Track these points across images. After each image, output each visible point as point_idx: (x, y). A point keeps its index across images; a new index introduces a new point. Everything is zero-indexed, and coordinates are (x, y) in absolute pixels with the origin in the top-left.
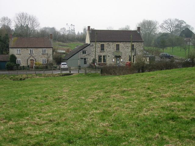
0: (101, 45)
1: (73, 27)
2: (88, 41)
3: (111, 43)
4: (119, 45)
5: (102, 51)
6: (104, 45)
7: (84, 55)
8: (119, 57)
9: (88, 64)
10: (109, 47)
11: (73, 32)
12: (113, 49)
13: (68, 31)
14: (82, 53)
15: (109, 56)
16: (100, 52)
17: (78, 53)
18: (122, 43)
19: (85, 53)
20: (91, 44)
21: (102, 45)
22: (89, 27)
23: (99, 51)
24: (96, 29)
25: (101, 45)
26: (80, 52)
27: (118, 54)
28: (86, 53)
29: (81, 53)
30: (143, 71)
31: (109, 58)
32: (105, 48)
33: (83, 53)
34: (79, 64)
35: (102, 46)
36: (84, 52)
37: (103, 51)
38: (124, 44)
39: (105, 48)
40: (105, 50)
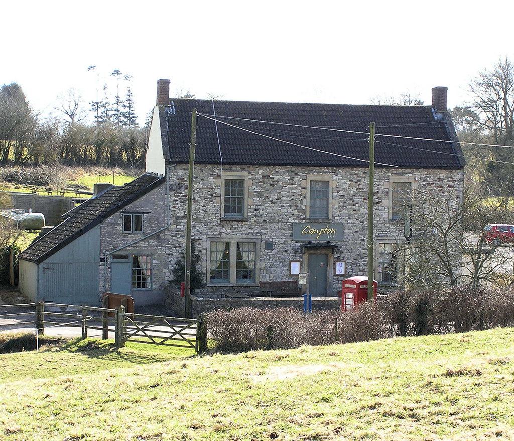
0: (227, 182)
1: (124, 84)
2: (156, 163)
3: (280, 175)
4: (241, 182)
5: (231, 215)
6: (246, 185)
7: (132, 237)
8: (330, 247)
9: (152, 285)
10: (274, 197)
11: (122, 110)
12: (294, 204)
13: (97, 105)
14: (120, 228)
15: (269, 246)
16: (222, 223)
17: (97, 227)
18: (342, 172)
19: (138, 227)
20: (173, 179)
21: (234, 182)
22: (163, 86)
23: (215, 218)
24: (201, 95)
25: (227, 182)
26: (110, 219)
27: (316, 234)
28: (145, 225)
29: (117, 224)
30: (422, 329)
31: (270, 253)
32: (250, 203)
33: (127, 227)
34: (102, 289)
35: (234, 190)
36: (133, 224)
37: (236, 215)
38: (355, 178)
39: (248, 201)
40: (248, 213)
